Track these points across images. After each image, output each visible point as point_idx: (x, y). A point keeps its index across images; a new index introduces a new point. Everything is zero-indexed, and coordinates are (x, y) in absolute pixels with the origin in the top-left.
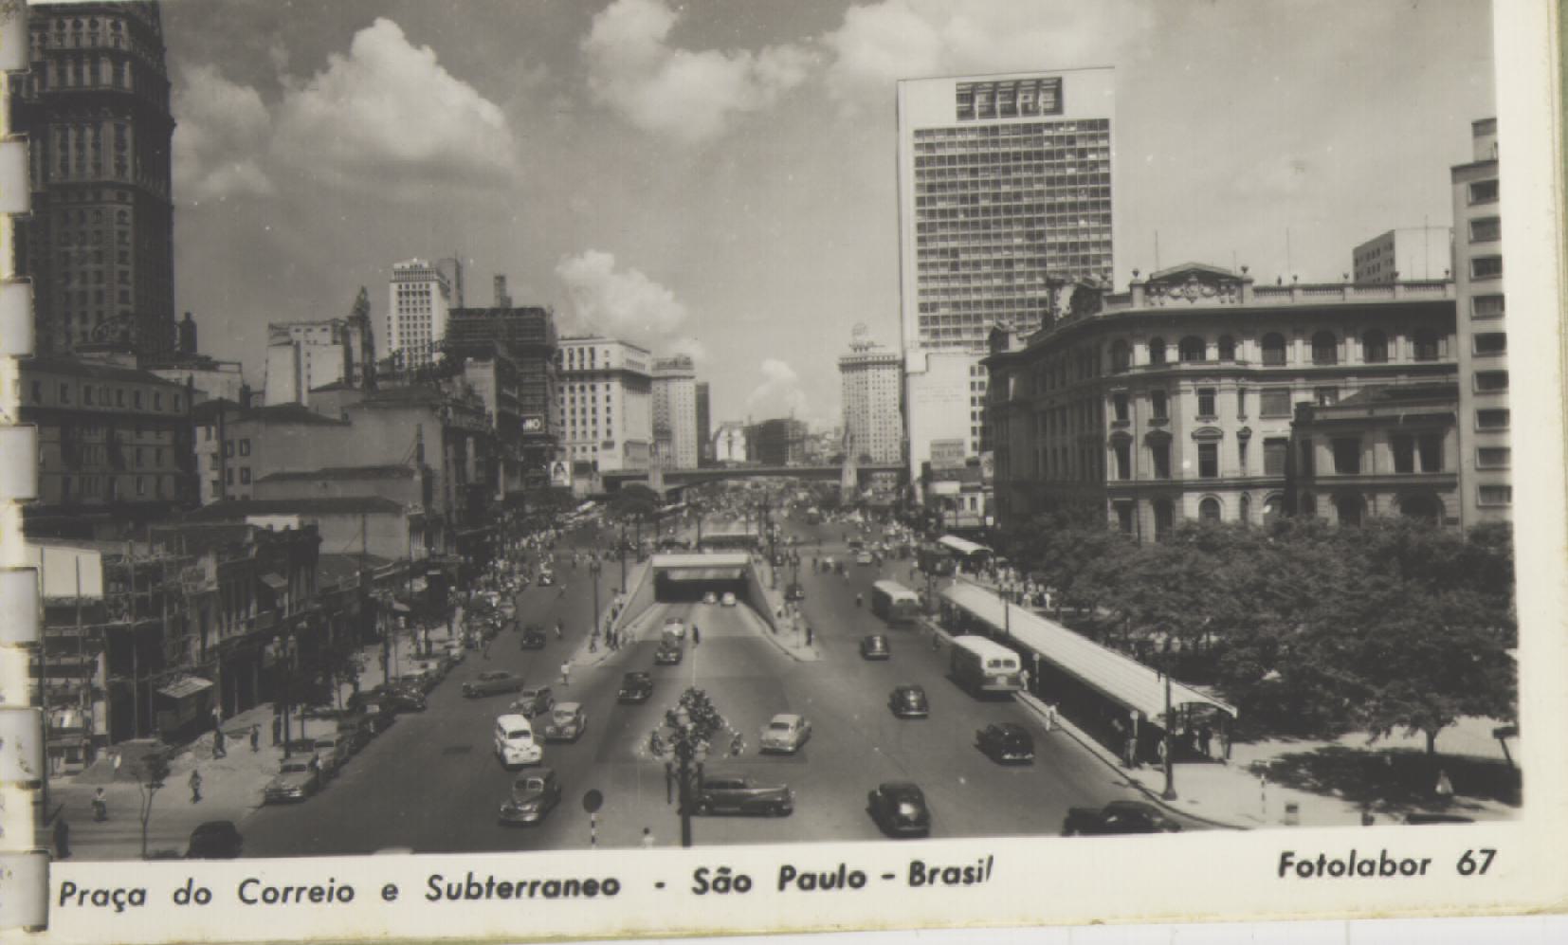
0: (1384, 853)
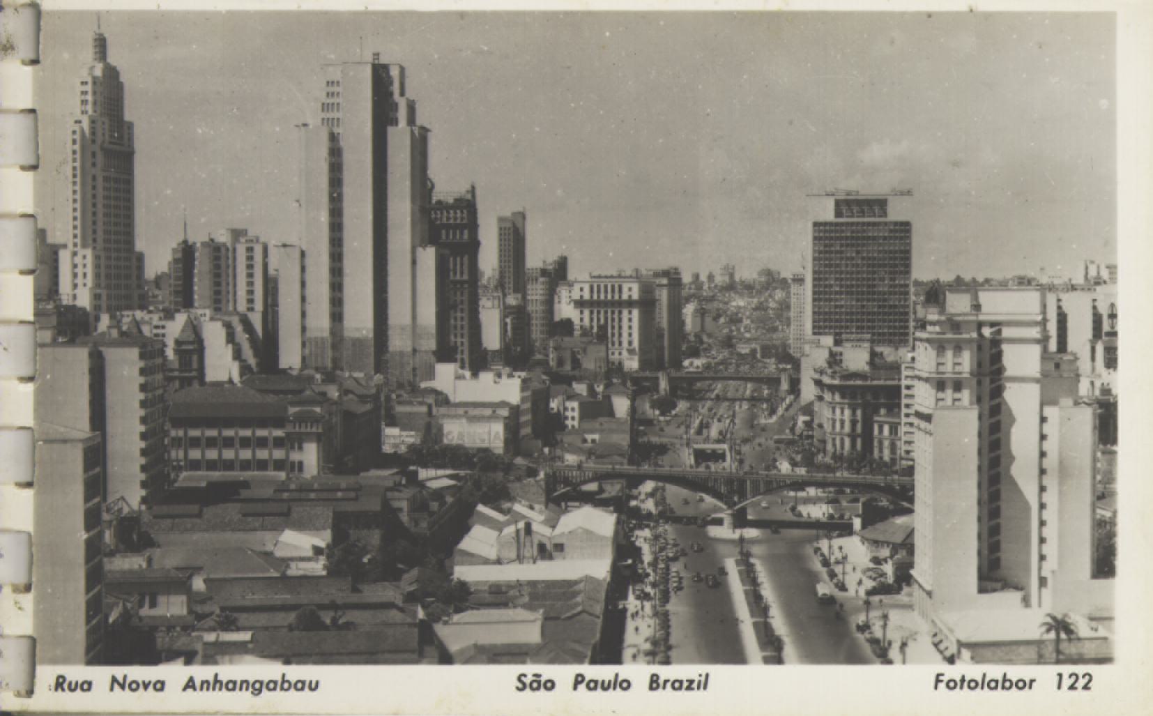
0: (1005, 675)
